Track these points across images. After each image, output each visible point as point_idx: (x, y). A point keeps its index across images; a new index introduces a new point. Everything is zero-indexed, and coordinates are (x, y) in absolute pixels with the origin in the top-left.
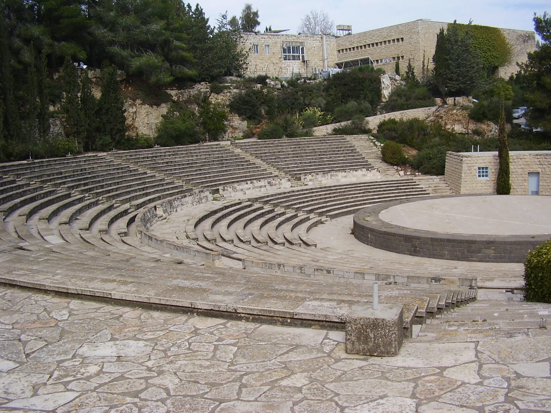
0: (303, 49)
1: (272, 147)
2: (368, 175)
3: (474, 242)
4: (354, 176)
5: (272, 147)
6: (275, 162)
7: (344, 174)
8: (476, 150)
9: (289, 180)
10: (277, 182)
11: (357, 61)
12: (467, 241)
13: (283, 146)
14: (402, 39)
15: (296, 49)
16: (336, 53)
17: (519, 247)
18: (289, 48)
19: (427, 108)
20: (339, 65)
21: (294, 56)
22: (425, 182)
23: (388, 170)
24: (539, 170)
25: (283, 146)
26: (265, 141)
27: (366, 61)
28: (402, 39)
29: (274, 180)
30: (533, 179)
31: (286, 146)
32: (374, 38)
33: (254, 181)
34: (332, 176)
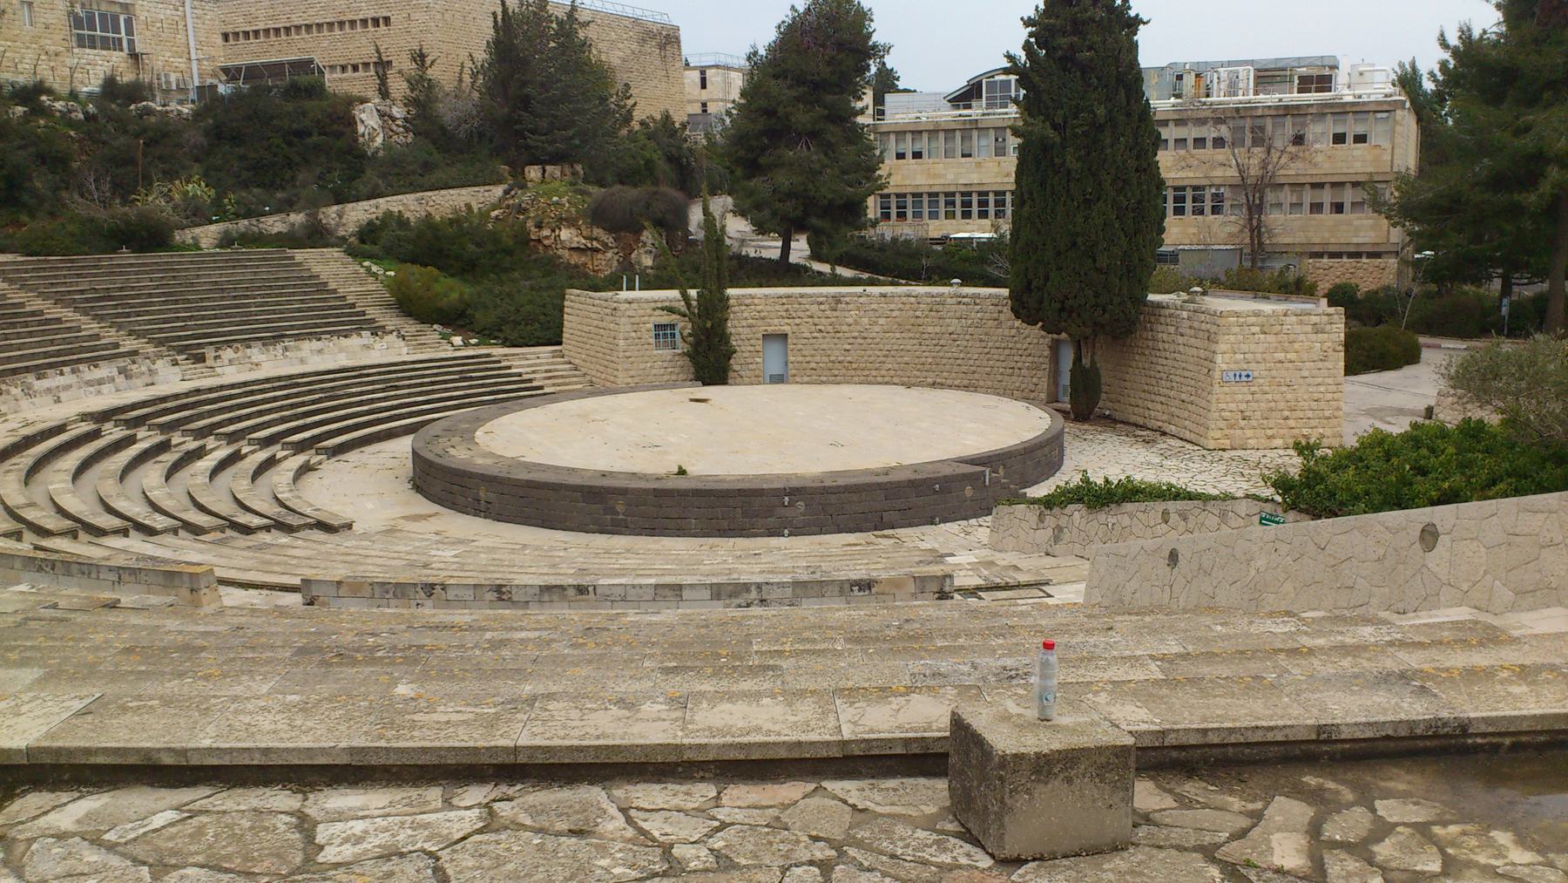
0: (129, 22)
1: (95, 275)
2: (377, 346)
3: (759, 493)
4: (341, 350)
5: (95, 275)
6: (118, 315)
7: (315, 344)
8: (631, 288)
9: (175, 363)
10: (144, 369)
11: (281, 65)
12: (741, 492)
13: (129, 273)
14: (387, 20)
15: (110, 22)
16: (219, 41)
17: (855, 497)
18: (91, 18)
19: (482, 189)
20: (231, 73)
21: (105, 40)
22: (529, 361)
23: (420, 333)
24: (787, 329)
25: (129, 273)
26: (73, 261)
27: (304, 66)
28: (387, 20)
29: (134, 362)
30: (774, 349)
31: (137, 273)
32: (311, 12)
33: (81, 367)
34: (286, 349)
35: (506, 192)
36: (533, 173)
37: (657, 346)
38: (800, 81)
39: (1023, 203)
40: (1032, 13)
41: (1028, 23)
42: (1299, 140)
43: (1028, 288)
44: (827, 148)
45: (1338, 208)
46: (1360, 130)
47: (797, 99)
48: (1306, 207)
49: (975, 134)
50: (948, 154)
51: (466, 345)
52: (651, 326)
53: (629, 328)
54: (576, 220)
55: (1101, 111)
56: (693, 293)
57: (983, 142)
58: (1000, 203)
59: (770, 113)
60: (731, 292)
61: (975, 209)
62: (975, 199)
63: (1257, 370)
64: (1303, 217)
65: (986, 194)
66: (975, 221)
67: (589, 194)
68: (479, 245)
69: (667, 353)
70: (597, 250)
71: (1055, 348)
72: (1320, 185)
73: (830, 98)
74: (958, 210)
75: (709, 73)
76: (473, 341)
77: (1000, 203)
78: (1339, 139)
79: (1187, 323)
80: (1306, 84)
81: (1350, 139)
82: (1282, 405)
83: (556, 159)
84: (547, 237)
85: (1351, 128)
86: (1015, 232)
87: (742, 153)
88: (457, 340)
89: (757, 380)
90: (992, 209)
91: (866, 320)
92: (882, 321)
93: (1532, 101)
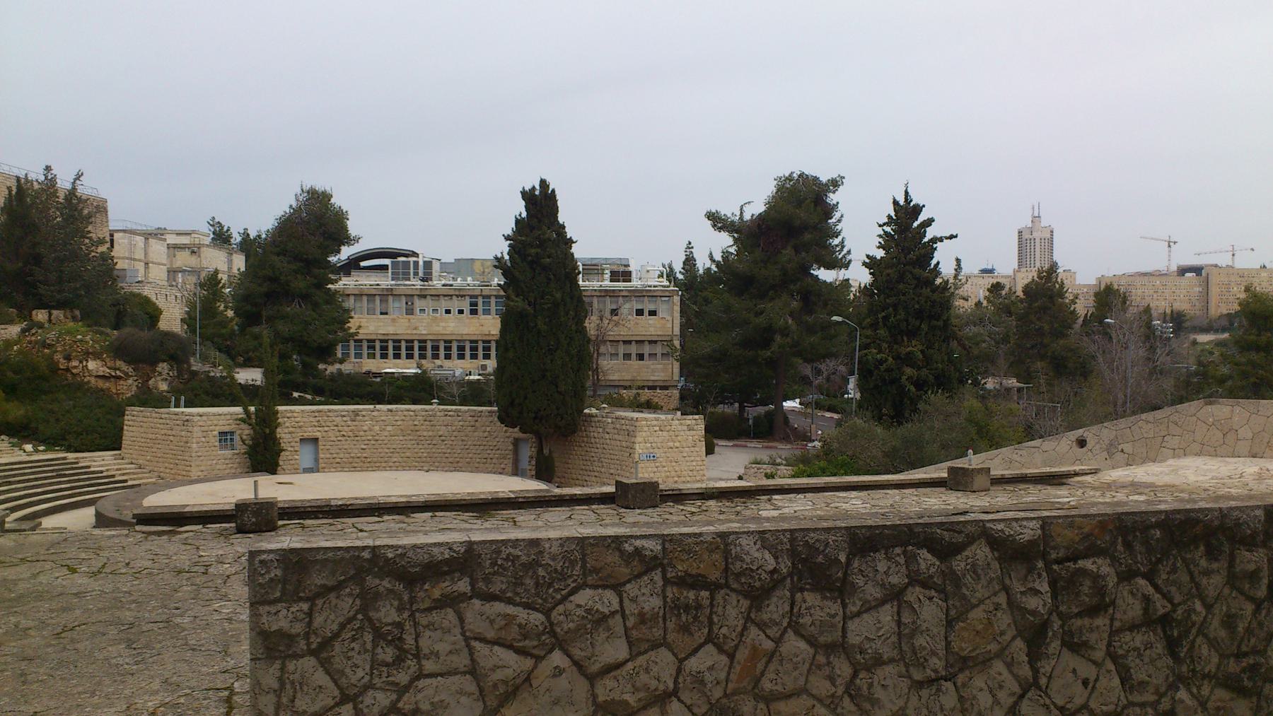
8: (177, 406)
24: (318, 434)
35: (23, 331)
36: (41, 315)
37: (221, 448)
38: (297, 258)
39: (507, 350)
40: (509, 232)
41: (507, 238)
42: (614, 312)
43: (512, 404)
44: (315, 306)
45: (641, 357)
46: (652, 307)
47: (296, 272)
48: (621, 356)
49: (391, 298)
50: (371, 312)
51: (37, 451)
52: (216, 433)
53: (200, 434)
54: (102, 354)
55: (558, 295)
56: (252, 409)
57: (397, 305)
58: (487, 349)
59: (273, 280)
60: (280, 408)
61: (391, 352)
62: (391, 345)
63: (658, 453)
64: (618, 363)
65: (399, 341)
66: (403, 361)
67: (107, 335)
68: (15, 373)
69: (228, 453)
70: (119, 378)
71: (516, 443)
72: (630, 342)
73: (316, 271)
74: (378, 352)
75: (116, 236)
76: (41, 448)
77: (487, 349)
78: (640, 312)
79: (611, 426)
80: (615, 276)
81: (646, 313)
82: (673, 473)
83: (60, 305)
84: (75, 367)
85: (648, 306)
86: (500, 370)
87: (248, 307)
88: (29, 447)
89: (296, 471)
90: (416, 352)
91: (377, 428)
92: (389, 428)
93: (762, 296)
